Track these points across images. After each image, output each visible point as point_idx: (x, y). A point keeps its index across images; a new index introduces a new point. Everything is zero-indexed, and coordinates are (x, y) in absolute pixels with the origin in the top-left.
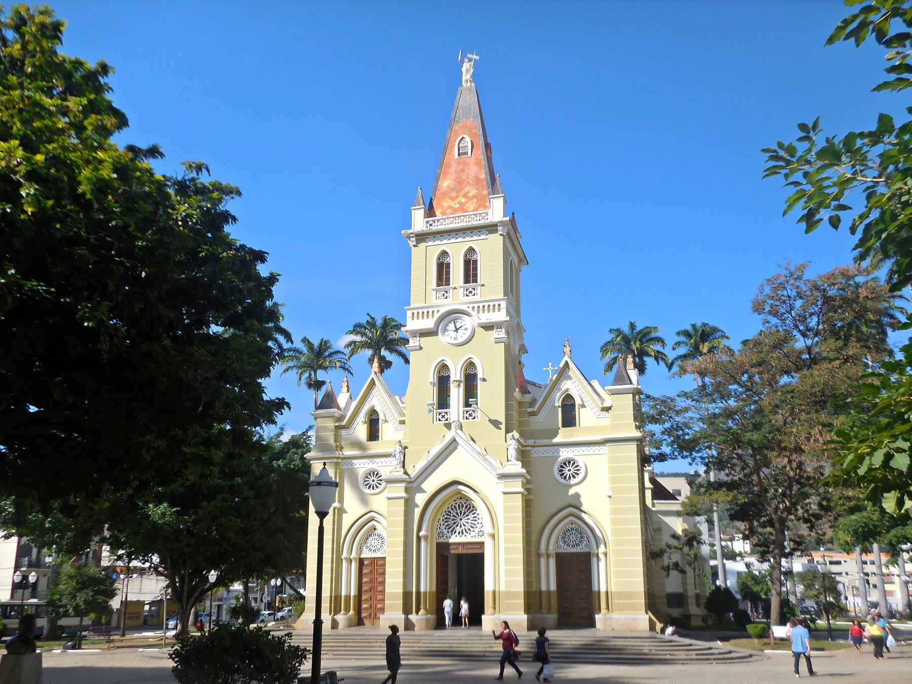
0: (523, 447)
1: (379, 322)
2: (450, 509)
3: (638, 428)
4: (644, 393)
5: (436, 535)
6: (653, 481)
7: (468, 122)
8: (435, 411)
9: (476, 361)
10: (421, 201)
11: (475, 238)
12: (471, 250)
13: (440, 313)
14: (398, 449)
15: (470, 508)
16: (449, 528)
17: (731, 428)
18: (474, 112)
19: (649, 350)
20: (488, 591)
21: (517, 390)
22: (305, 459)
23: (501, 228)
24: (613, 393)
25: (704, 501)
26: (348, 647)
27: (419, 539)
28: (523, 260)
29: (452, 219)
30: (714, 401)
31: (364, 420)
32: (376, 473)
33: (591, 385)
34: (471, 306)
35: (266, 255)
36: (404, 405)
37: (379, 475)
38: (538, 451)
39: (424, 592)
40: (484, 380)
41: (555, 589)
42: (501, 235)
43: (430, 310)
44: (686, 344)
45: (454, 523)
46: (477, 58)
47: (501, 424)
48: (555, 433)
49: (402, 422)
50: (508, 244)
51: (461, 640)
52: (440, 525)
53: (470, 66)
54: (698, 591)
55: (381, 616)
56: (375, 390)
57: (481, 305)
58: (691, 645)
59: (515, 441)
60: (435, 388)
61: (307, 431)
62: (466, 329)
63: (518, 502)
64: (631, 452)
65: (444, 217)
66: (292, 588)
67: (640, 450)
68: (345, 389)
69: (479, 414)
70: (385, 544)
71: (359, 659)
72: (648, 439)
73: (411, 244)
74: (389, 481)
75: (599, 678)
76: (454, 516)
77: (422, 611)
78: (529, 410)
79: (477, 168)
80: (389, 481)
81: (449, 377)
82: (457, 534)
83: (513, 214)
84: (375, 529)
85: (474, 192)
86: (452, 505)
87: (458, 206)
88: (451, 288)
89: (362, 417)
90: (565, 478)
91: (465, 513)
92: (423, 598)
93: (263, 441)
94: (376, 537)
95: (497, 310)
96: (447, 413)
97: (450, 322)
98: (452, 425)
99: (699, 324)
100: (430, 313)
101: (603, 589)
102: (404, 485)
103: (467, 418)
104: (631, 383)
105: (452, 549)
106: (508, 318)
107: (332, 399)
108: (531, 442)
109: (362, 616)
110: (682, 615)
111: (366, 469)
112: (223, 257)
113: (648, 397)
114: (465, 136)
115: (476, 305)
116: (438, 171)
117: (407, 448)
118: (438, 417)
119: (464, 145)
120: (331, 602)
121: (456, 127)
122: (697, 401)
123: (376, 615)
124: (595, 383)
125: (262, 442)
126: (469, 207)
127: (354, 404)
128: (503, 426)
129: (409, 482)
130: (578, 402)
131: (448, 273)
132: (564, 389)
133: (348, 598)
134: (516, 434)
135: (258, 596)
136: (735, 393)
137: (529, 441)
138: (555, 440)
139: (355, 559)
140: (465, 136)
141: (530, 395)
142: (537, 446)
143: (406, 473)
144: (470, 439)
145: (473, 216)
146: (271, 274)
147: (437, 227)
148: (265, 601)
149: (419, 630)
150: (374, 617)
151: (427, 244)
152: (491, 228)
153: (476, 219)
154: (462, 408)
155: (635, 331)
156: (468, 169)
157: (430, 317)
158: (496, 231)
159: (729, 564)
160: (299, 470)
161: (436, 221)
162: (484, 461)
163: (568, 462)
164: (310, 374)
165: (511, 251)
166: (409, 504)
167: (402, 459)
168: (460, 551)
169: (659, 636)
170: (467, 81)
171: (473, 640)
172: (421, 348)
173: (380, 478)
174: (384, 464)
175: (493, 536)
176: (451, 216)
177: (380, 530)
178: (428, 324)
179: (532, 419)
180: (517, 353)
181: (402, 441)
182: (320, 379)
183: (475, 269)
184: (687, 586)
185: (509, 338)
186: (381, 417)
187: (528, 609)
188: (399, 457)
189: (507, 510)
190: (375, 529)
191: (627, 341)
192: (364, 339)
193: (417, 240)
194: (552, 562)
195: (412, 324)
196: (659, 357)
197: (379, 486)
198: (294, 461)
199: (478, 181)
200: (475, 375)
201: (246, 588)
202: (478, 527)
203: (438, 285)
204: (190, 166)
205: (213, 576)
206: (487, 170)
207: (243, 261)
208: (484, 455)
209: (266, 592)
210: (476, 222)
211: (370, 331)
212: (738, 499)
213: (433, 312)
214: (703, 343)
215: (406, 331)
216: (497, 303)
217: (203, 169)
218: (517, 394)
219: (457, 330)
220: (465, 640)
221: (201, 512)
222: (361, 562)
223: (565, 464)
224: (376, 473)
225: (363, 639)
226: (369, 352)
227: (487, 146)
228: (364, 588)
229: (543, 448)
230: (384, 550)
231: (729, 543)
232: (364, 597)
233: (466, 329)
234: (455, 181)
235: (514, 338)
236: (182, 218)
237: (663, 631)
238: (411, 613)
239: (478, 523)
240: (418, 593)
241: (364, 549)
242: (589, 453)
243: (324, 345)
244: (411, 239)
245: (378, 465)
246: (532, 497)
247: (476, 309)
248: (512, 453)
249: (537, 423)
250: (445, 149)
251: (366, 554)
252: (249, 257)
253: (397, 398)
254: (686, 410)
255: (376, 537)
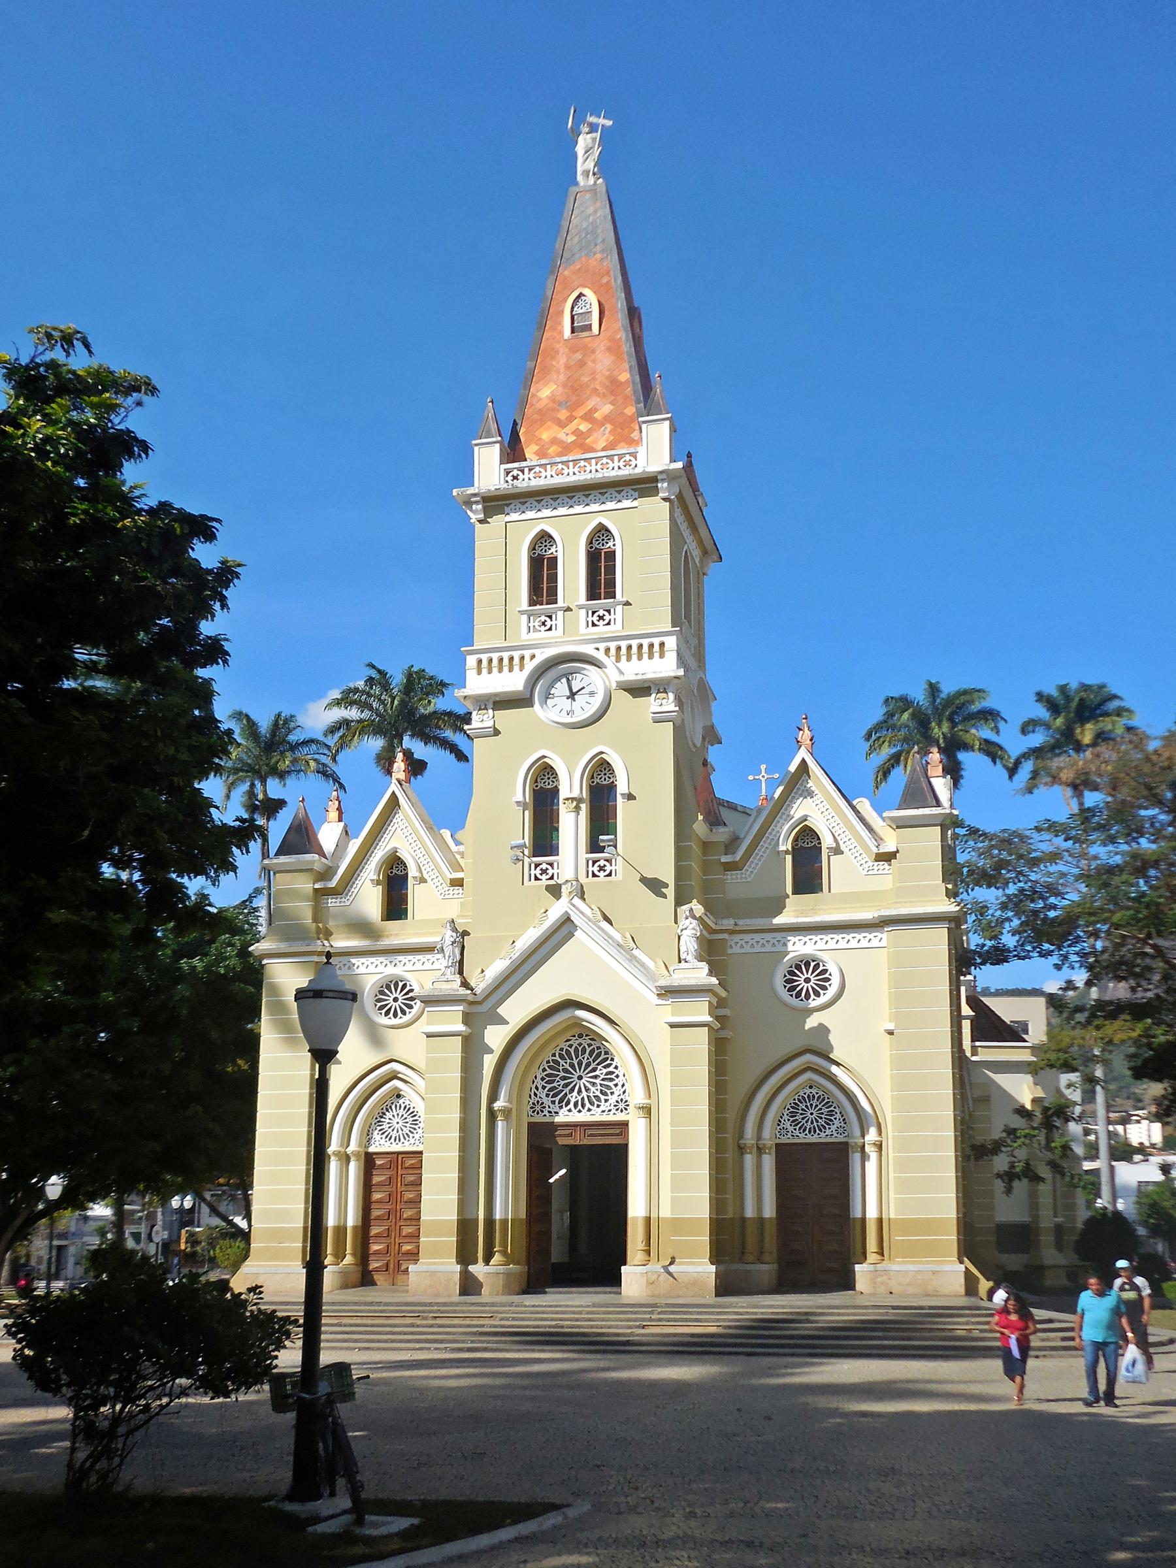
0: (711, 933)
1: (398, 679)
2: (557, 1058)
3: (952, 894)
4: (967, 823)
5: (527, 1109)
6: (973, 1002)
7: (593, 262)
8: (527, 860)
9: (615, 759)
10: (494, 427)
11: (611, 505)
12: (602, 532)
13: (536, 662)
14: (449, 936)
15: (599, 1055)
16: (555, 1096)
17: (1143, 894)
18: (603, 241)
19: (967, 738)
20: (635, 1219)
21: (700, 817)
22: (250, 954)
23: (665, 485)
24: (901, 825)
25: (1092, 1041)
26: (345, 1326)
27: (492, 1115)
28: (711, 551)
29: (560, 466)
30: (1112, 840)
31: (375, 877)
32: (401, 984)
33: (853, 808)
34: (602, 646)
35: (214, 524)
36: (461, 848)
37: (408, 988)
38: (742, 942)
39: (501, 1220)
40: (630, 797)
41: (774, 1215)
42: (665, 499)
43: (516, 655)
44: (1048, 726)
45: (566, 1085)
46: (609, 123)
47: (666, 886)
48: (778, 906)
49: (458, 883)
50: (680, 519)
51: (580, 1313)
52: (537, 1088)
53: (594, 140)
54: (1059, 1220)
55: (412, 1268)
56: (398, 819)
57: (624, 644)
58: (1050, 1321)
59: (695, 922)
60: (527, 812)
61: (251, 898)
62: (592, 694)
63: (700, 1041)
64: (938, 939)
65: (543, 461)
66: (214, 1211)
67: (955, 940)
68: (333, 815)
69: (619, 866)
70: (421, 1125)
71: (368, 1349)
72: (971, 918)
73: (474, 517)
74: (428, 1001)
75: (869, 1383)
76: (566, 1071)
77: (497, 1258)
78: (724, 859)
79: (613, 358)
80: (428, 1001)
81: (556, 791)
82: (571, 1106)
83: (689, 456)
84: (399, 1096)
85: (607, 409)
86: (562, 1049)
87: (574, 438)
88: (560, 609)
89: (371, 869)
90: (798, 995)
91: (588, 1065)
92: (501, 1229)
93: (210, 905)
94: (401, 1112)
95: (657, 655)
96: (551, 865)
97: (559, 679)
98: (564, 889)
99: (1074, 685)
100: (516, 661)
101: (872, 1213)
102: (461, 1008)
103: (594, 875)
104: (938, 804)
105: (560, 1135)
106: (681, 672)
107: (308, 835)
108: (728, 923)
109: (371, 1268)
110: (1026, 1266)
111: (383, 975)
112: (125, 527)
113: (973, 832)
114: (586, 291)
115: (613, 646)
116: (530, 364)
117: (468, 934)
118: (533, 872)
119: (584, 310)
120: (305, 1241)
121: (566, 273)
122: (1076, 840)
123: (399, 1265)
124: (864, 805)
125: (208, 908)
126: (595, 442)
127: (354, 846)
128: (670, 892)
129: (472, 1003)
130: (827, 841)
131: (553, 578)
132: (797, 816)
133: (341, 1230)
134: (699, 909)
135: (143, 1229)
136: (1152, 825)
137: (725, 922)
138: (779, 920)
139: (357, 1154)
140: (586, 291)
141: (727, 830)
142: (740, 932)
143: (465, 984)
144: (600, 917)
145: (605, 460)
146: (222, 563)
147: (528, 481)
148: (157, 1239)
149: (491, 1294)
150: (396, 1270)
151: (508, 518)
152: (644, 485)
153: (611, 465)
154: (584, 855)
155: (938, 701)
156: (594, 361)
157: (516, 668)
158: (654, 492)
159: (1122, 1168)
160: (238, 977)
161: (526, 470)
162: (630, 961)
163: (805, 963)
164: (253, 785)
165: (686, 532)
166: (472, 1047)
167: (458, 957)
168: (578, 1140)
169: (986, 1304)
170: (586, 173)
171: (604, 1313)
172: (497, 732)
173: (411, 995)
174: (418, 966)
175: (647, 1110)
176: (558, 460)
177: (411, 1097)
178: (513, 682)
179: (730, 876)
180: (699, 742)
181: (458, 921)
182: (273, 794)
183: (611, 570)
184: (1038, 1210)
185: (683, 712)
186: (412, 872)
187: (717, 1256)
188: (451, 952)
189: (676, 1061)
190: (399, 1096)
191: (922, 722)
192: (366, 714)
193: (485, 510)
194: (769, 1161)
195: (478, 684)
196: (992, 751)
197: (400, 1014)
198: (226, 959)
199: (614, 386)
200: (612, 787)
201: (120, 1213)
202: (617, 1093)
203: (532, 603)
204: (49, 336)
205: (55, 1186)
206: (634, 362)
207: (167, 535)
208: (627, 950)
209: (160, 1223)
210: (614, 471)
211: (380, 699)
212: (1154, 1037)
213: (522, 658)
214: (1082, 725)
215: (465, 697)
216: (656, 641)
217: (75, 342)
218: (699, 825)
219: (572, 695)
220: (588, 1313)
221: (27, 1060)
222: (369, 1161)
223: (798, 967)
224: (401, 984)
225: (375, 1311)
226: (376, 744)
227: (633, 313)
228: (375, 1213)
229: (753, 936)
230: (417, 1136)
231: (1120, 1128)
232: (374, 1231)
233: (592, 694)
234: (564, 386)
235: (693, 717)
236: (36, 444)
237: (991, 1293)
238: (475, 1262)
239: (616, 1085)
240: (490, 1222)
241: (376, 1135)
242: (838, 946)
243: (282, 725)
244: (474, 507)
245: (405, 968)
246: (728, 1034)
247: (613, 651)
248: (689, 944)
249: (739, 884)
250: (543, 318)
251: (380, 1145)
252: (182, 528)
253: (446, 834)
254: (1054, 857)
255: (401, 1112)
